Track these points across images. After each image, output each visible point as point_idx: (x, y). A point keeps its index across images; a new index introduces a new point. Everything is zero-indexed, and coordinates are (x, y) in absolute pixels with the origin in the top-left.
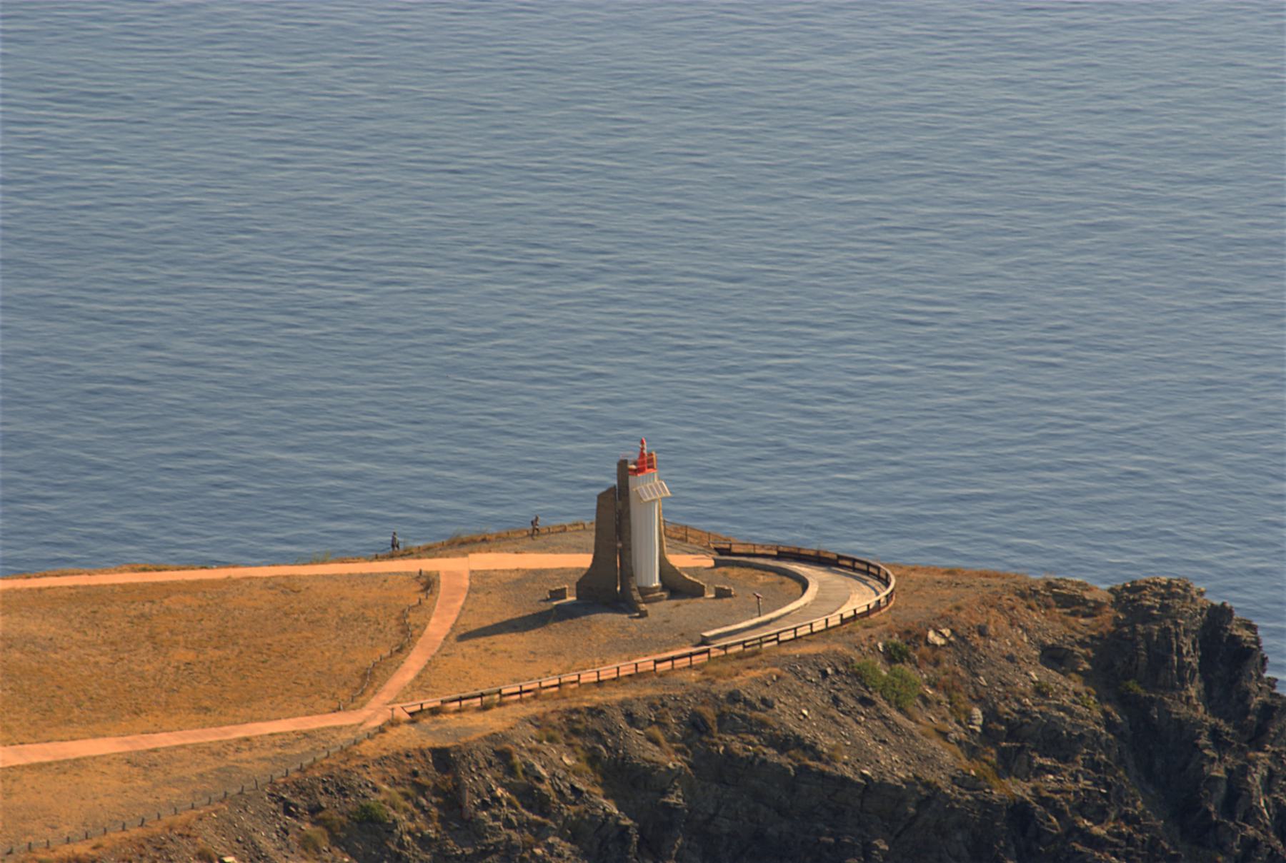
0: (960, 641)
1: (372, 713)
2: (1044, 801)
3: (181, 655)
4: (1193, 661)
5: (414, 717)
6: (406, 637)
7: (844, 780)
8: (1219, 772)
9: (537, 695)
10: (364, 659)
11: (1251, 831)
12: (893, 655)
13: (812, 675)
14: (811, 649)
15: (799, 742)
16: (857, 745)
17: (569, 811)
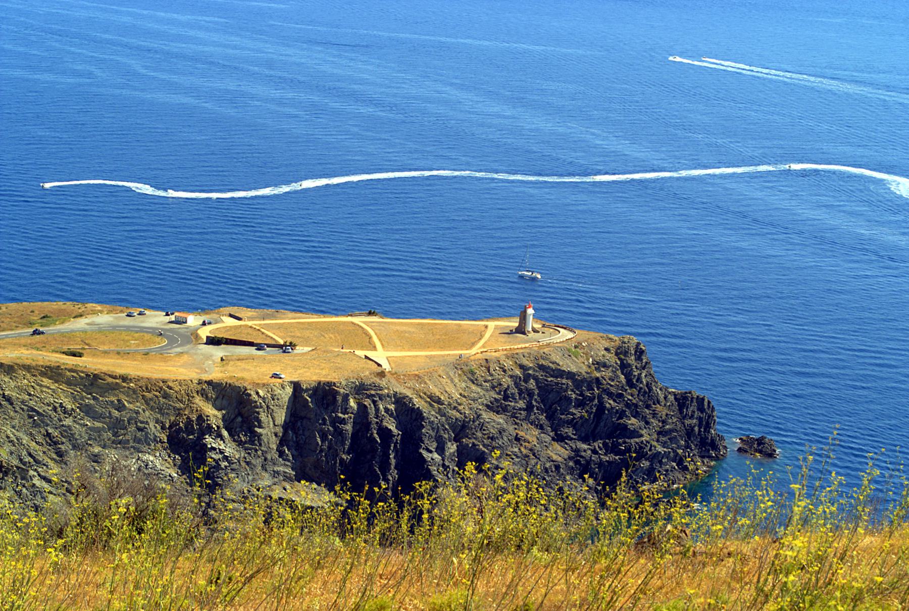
0: (588, 345)
1: (474, 351)
2: (602, 377)
3: (438, 337)
4: (633, 352)
5: (482, 352)
6: (481, 337)
7: (564, 371)
8: (636, 374)
9: (506, 350)
10: (473, 340)
11: (641, 385)
12: (576, 347)
13: (559, 350)
14: (559, 345)
15: (556, 363)
16: (567, 364)
17: (510, 373)
